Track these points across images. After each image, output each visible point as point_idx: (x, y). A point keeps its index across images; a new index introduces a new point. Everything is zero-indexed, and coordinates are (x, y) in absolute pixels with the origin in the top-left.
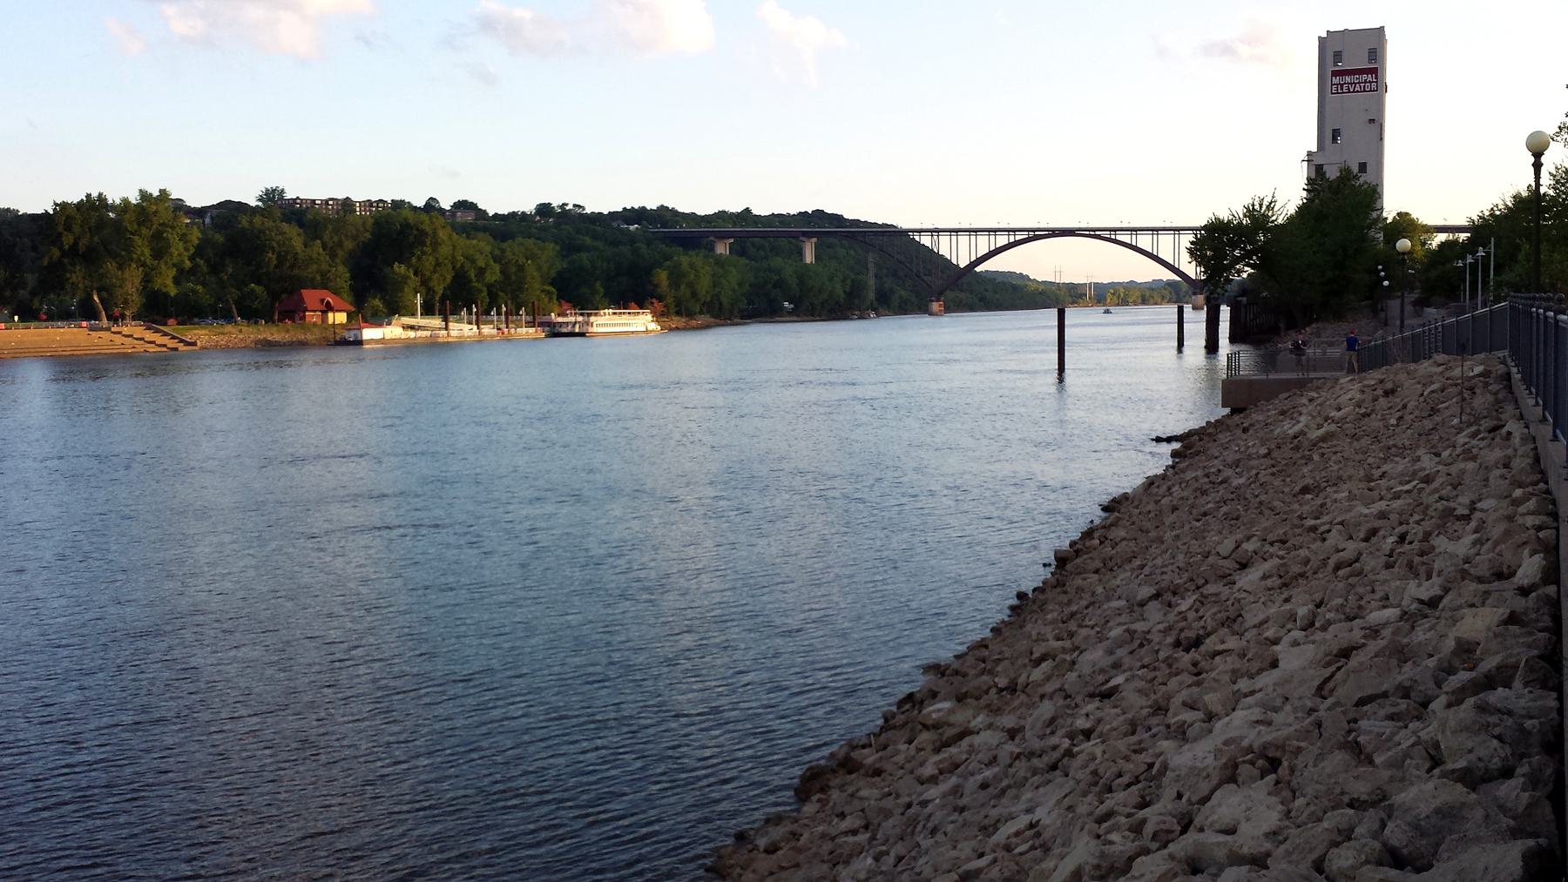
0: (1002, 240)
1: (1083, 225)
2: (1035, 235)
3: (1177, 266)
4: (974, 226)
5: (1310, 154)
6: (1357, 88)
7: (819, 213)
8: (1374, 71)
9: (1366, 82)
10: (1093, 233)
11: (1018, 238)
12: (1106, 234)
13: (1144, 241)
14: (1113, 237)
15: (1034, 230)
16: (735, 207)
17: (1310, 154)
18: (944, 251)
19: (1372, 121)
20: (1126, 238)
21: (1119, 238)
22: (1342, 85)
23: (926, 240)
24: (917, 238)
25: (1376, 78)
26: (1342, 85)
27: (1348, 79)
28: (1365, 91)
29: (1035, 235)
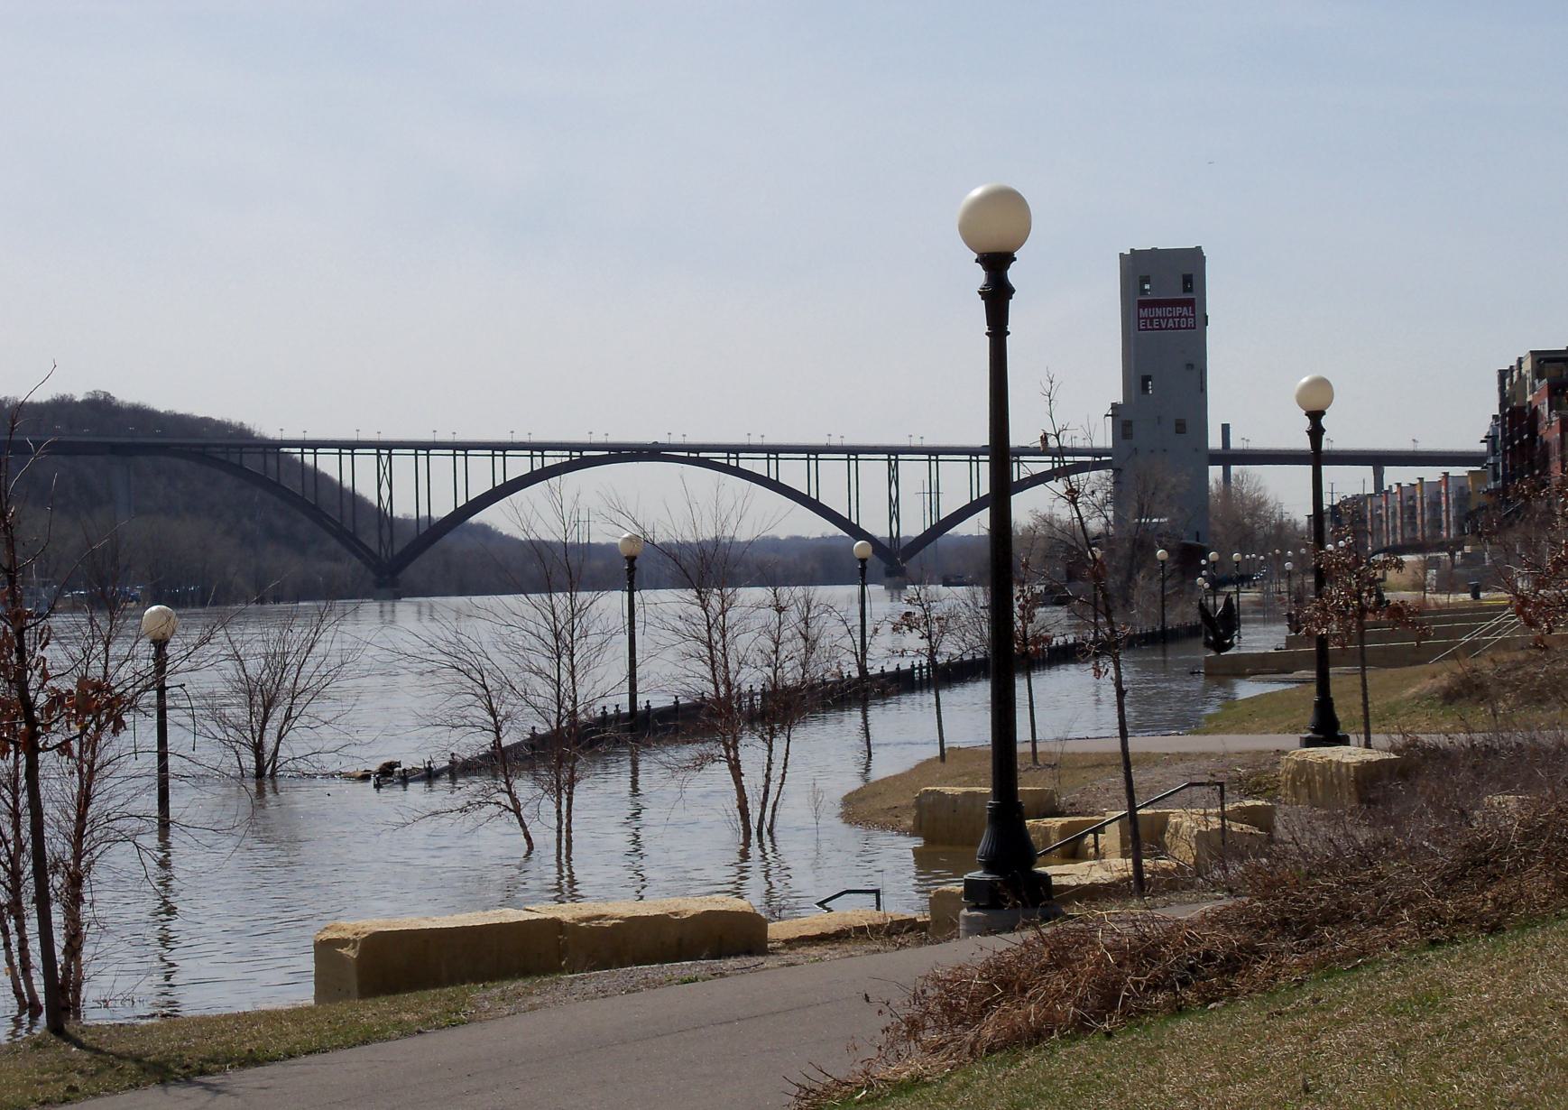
0: (519, 466)
1: (677, 439)
2: (583, 457)
3: (813, 496)
4: (461, 437)
5: (1114, 406)
6: (1171, 324)
7: (101, 408)
8: (1190, 303)
9: (1180, 317)
10: (694, 455)
11: (549, 462)
12: (720, 457)
13: (792, 472)
14: (733, 463)
15: (580, 447)
16: (364, 495)
17: (1114, 406)
18: (366, 488)
19: (1190, 366)
20: (758, 465)
21: (744, 465)
22: (1151, 319)
23: (327, 464)
24: (309, 459)
25: (1193, 312)
26: (1151, 319)
27: (1159, 312)
28: (1180, 328)
29: (583, 457)
